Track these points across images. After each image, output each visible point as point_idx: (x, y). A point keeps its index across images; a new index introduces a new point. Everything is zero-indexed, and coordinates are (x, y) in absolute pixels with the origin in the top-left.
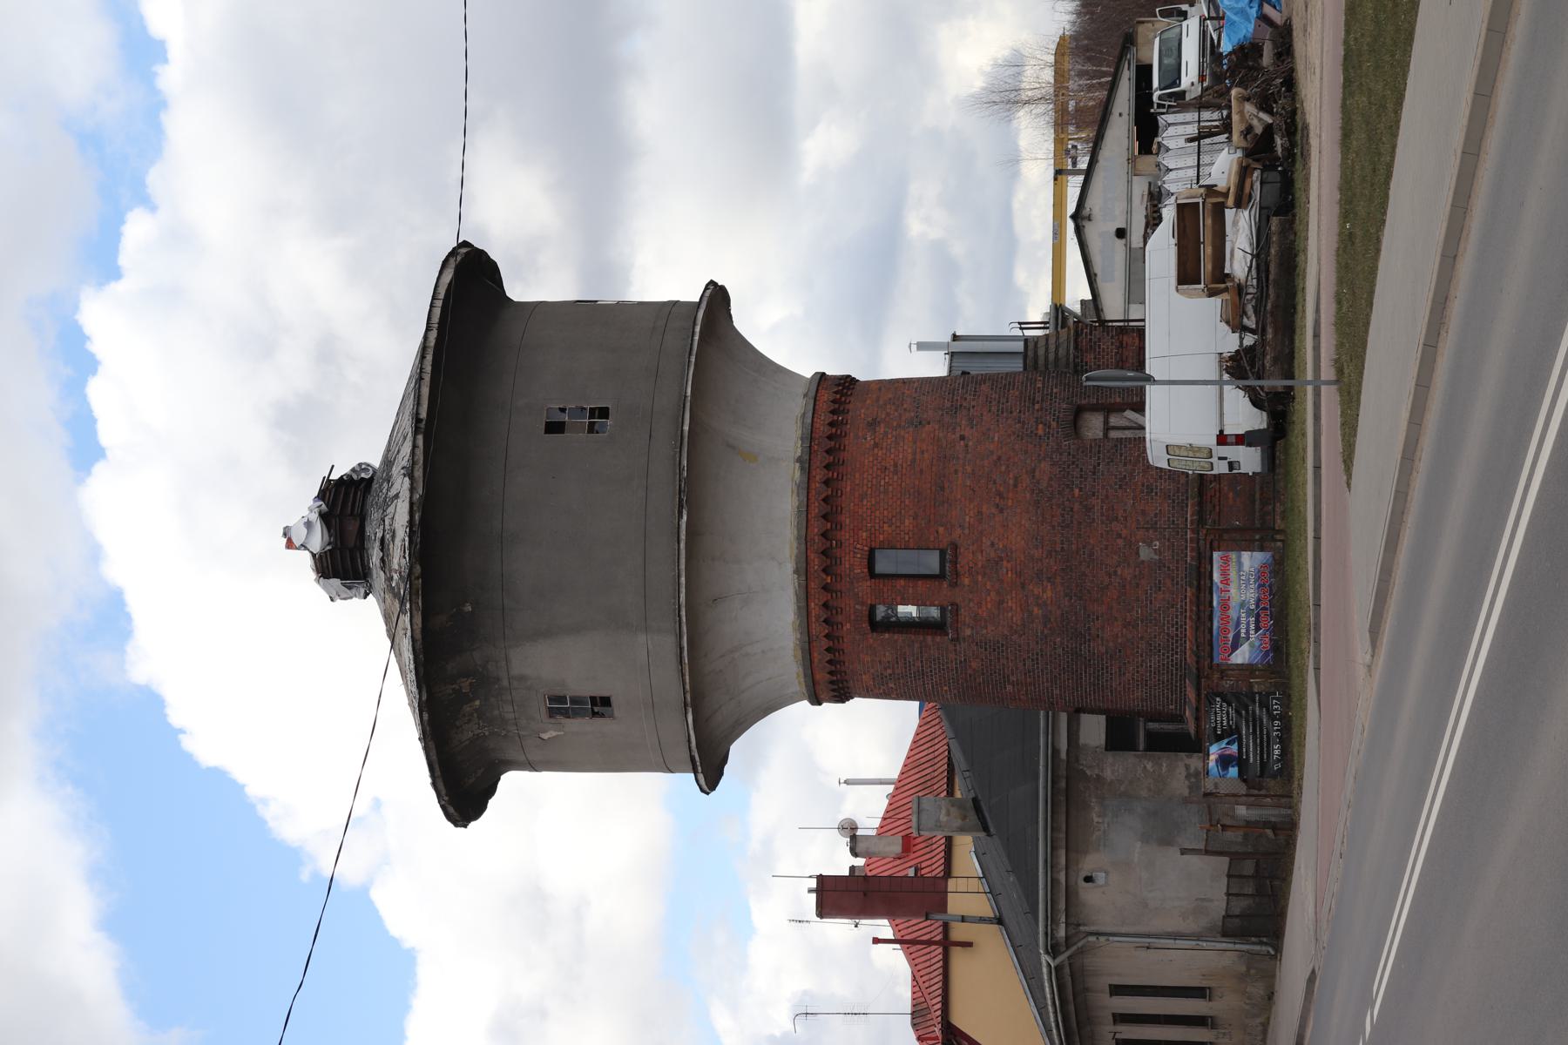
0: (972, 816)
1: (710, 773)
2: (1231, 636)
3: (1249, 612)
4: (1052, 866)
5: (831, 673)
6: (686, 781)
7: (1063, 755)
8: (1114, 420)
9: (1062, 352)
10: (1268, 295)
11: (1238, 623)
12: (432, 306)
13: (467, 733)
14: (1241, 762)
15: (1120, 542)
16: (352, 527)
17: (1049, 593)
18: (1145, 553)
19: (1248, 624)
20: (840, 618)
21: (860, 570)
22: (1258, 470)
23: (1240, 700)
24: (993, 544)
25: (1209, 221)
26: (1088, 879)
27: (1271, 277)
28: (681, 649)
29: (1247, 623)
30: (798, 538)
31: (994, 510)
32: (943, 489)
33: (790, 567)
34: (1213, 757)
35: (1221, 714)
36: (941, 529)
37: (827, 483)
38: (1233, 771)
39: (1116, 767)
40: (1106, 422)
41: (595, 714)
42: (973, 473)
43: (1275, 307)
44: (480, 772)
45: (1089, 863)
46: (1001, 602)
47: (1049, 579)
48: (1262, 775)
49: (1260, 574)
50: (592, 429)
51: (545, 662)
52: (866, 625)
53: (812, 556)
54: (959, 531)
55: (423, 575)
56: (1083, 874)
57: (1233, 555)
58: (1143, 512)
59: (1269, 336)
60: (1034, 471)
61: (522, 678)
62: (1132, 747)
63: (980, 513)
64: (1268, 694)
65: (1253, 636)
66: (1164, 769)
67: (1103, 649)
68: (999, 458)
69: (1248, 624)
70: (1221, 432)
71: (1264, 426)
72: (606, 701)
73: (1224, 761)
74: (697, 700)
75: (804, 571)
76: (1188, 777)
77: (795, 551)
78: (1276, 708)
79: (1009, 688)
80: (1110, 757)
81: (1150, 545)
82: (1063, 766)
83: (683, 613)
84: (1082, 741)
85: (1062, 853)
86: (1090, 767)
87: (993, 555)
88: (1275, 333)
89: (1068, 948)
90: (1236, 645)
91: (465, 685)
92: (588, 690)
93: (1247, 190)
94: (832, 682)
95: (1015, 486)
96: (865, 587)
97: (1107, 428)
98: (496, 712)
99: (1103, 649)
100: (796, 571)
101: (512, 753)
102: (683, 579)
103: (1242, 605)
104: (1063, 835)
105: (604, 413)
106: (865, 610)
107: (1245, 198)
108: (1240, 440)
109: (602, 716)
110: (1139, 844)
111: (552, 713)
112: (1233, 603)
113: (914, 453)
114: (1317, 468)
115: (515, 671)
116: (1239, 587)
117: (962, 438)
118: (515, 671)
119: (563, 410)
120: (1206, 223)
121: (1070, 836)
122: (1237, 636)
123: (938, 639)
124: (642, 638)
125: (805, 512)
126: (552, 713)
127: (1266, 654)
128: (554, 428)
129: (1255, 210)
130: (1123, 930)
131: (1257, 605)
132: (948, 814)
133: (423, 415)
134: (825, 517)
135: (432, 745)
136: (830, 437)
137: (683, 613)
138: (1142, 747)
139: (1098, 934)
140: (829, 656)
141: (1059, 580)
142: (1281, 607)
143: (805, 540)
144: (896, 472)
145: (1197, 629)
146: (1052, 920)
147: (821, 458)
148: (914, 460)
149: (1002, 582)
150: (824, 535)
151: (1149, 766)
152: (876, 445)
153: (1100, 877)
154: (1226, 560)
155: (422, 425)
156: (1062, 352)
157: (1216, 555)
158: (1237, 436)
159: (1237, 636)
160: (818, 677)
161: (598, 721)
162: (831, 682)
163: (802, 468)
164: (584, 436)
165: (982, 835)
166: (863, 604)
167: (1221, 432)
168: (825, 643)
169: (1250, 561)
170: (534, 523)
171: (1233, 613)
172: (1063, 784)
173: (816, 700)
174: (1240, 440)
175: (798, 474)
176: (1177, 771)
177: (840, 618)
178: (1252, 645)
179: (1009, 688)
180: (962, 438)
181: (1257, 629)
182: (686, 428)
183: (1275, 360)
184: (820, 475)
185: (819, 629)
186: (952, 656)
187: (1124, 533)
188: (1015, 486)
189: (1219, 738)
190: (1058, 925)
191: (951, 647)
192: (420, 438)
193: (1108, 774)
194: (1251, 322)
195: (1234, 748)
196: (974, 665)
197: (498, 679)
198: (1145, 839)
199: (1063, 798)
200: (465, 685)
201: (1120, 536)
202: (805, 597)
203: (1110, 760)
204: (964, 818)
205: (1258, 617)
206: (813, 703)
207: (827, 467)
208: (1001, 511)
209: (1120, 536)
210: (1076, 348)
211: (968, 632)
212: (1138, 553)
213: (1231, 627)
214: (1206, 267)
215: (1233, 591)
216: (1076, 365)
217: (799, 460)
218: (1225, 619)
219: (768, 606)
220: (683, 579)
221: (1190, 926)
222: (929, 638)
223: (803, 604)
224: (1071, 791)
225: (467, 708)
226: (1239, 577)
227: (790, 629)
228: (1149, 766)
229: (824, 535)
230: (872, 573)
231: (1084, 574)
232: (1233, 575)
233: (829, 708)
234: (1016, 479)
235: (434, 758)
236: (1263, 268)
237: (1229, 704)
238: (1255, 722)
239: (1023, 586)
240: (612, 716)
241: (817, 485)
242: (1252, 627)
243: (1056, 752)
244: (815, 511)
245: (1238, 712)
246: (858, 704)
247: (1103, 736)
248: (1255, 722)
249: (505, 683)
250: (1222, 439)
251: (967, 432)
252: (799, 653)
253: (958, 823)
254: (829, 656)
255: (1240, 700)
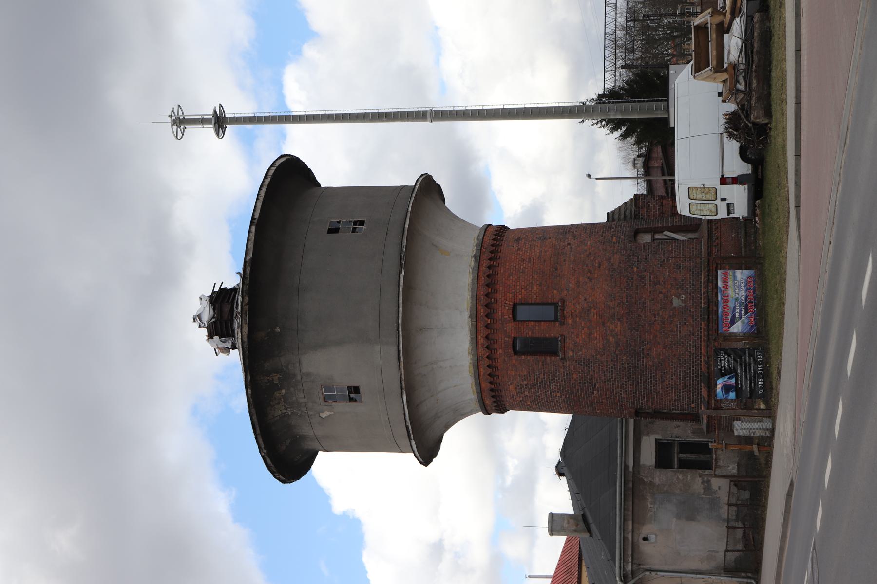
0: (582, 524)
1: (427, 455)
2: (729, 317)
3: (741, 304)
4: (623, 529)
5: (491, 383)
6: (409, 459)
7: (631, 469)
8: (657, 236)
9: (628, 212)
10: (753, 61)
11: (734, 310)
12: (270, 169)
13: (277, 411)
14: (738, 390)
15: (661, 296)
16: (226, 309)
17: (619, 328)
18: (676, 302)
19: (740, 310)
20: (496, 346)
21: (508, 316)
22: (746, 215)
23: (737, 354)
24: (585, 299)
25: (714, 36)
26: (645, 539)
27: (755, 50)
28: (399, 352)
29: (739, 310)
30: (472, 297)
31: (586, 280)
32: (557, 269)
33: (467, 314)
34: (719, 386)
35: (724, 361)
36: (555, 291)
37: (489, 267)
38: (732, 395)
39: (661, 477)
40: (653, 236)
41: (351, 399)
42: (575, 261)
43: (758, 66)
44: (288, 442)
45: (646, 530)
46: (590, 334)
47: (619, 320)
48: (751, 397)
49: (748, 282)
50: (354, 231)
51: (323, 364)
52: (511, 351)
53: (480, 307)
54: (566, 292)
55: (250, 303)
56: (642, 536)
57: (731, 272)
58: (675, 279)
59: (754, 84)
60: (610, 259)
61: (308, 374)
62: (670, 466)
63: (578, 282)
64: (754, 349)
65: (744, 317)
66: (689, 478)
67: (651, 363)
68: (590, 253)
69: (740, 310)
70: (723, 176)
71: (750, 172)
72: (356, 390)
73: (727, 389)
74: (410, 387)
75: (475, 316)
76: (703, 482)
77: (470, 305)
78: (760, 357)
79: (596, 392)
80: (658, 472)
81: (679, 297)
82: (630, 478)
83: (400, 329)
84: (641, 463)
85: (630, 523)
86: (646, 477)
87: (585, 305)
88: (758, 83)
89: (633, 578)
90: (733, 322)
91: (276, 378)
92: (344, 381)
93: (738, 5)
94: (492, 390)
95: (599, 267)
96: (510, 327)
97: (654, 240)
98: (294, 398)
99: (651, 363)
100: (470, 317)
101: (313, 445)
102: (401, 309)
103: (736, 300)
104: (630, 513)
105: (362, 223)
106: (510, 341)
107: (737, 11)
108: (735, 181)
109: (356, 400)
110: (675, 520)
111: (326, 399)
112: (730, 299)
113: (541, 252)
114: (798, 50)
115: (304, 370)
116: (735, 290)
117: (569, 244)
118: (304, 370)
119: (339, 223)
120: (712, 35)
121: (635, 513)
122: (734, 317)
123: (553, 358)
124: (377, 348)
125: (476, 282)
126: (326, 399)
127: (752, 327)
128: (333, 230)
129: (744, 17)
130: (666, 568)
131: (746, 300)
132: (568, 523)
133: (257, 216)
134: (488, 285)
135: (253, 410)
136: (493, 245)
137: (400, 329)
138: (676, 466)
139: (651, 571)
140: (489, 371)
141: (625, 320)
142: (764, 304)
143: (476, 298)
144: (530, 262)
145: (708, 346)
146: (623, 559)
147: (487, 255)
148: (540, 256)
149: (591, 321)
150: (487, 295)
151: (680, 477)
152: (519, 249)
153: (652, 538)
154: (726, 275)
155: (256, 221)
156: (628, 212)
157: (719, 272)
158: (733, 178)
159: (734, 317)
160: (483, 386)
161: (353, 403)
162: (494, 400)
163: (475, 260)
164: (350, 234)
165: (587, 535)
166: (509, 337)
167: (723, 176)
168: (487, 362)
169: (741, 275)
170: (328, 310)
171: (731, 305)
172: (631, 485)
173: (487, 412)
174: (735, 181)
175: (473, 263)
176: (695, 481)
177: (496, 346)
178: (743, 322)
179: (596, 392)
180: (569, 244)
181: (746, 313)
182: (407, 226)
183: (758, 99)
184: (485, 263)
185: (483, 353)
186: (561, 370)
187: (664, 291)
188: (599, 267)
189: (723, 375)
190: (627, 563)
191: (561, 364)
192: (253, 228)
193: (657, 481)
194: (741, 87)
195: (733, 381)
196: (575, 376)
197: (295, 375)
198: (678, 517)
199: (630, 493)
200: (276, 378)
201: (661, 293)
202: (475, 340)
203: (658, 473)
204: (577, 525)
205: (746, 306)
206: (485, 413)
207: (490, 259)
208: (591, 280)
209: (661, 293)
210: (636, 206)
211: (571, 354)
212: (672, 303)
213: (730, 312)
214: (713, 61)
215: (730, 291)
216: (636, 215)
217: (475, 256)
218: (726, 308)
219: (452, 344)
220: (401, 309)
221: (705, 566)
222: (548, 358)
223: (474, 336)
224: (635, 488)
225: (277, 394)
226: (736, 285)
227: (467, 353)
228: (680, 477)
229: (487, 295)
230: (514, 318)
231: (640, 316)
232: (730, 282)
233: (495, 416)
234: (600, 263)
235: (255, 420)
236: (749, 46)
237: (729, 355)
238: (746, 365)
239: (603, 323)
240: (361, 401)
241: (484, 268)
242: (743, 311)
243: (626, 467)
244: (482, 282)
245: (735, 360)
246: (511, 414)
247: (654, 460)
248: (746, 365)
249: (299, 378)
250: (724, 181)
251: (572, 242)
252: (472, 369)
253: (574, 528)
254: (489, 371)
255: (737, 354)
